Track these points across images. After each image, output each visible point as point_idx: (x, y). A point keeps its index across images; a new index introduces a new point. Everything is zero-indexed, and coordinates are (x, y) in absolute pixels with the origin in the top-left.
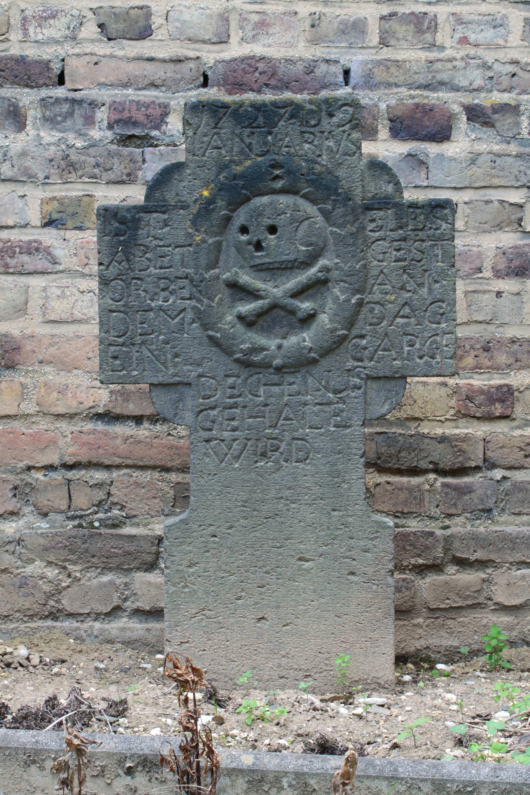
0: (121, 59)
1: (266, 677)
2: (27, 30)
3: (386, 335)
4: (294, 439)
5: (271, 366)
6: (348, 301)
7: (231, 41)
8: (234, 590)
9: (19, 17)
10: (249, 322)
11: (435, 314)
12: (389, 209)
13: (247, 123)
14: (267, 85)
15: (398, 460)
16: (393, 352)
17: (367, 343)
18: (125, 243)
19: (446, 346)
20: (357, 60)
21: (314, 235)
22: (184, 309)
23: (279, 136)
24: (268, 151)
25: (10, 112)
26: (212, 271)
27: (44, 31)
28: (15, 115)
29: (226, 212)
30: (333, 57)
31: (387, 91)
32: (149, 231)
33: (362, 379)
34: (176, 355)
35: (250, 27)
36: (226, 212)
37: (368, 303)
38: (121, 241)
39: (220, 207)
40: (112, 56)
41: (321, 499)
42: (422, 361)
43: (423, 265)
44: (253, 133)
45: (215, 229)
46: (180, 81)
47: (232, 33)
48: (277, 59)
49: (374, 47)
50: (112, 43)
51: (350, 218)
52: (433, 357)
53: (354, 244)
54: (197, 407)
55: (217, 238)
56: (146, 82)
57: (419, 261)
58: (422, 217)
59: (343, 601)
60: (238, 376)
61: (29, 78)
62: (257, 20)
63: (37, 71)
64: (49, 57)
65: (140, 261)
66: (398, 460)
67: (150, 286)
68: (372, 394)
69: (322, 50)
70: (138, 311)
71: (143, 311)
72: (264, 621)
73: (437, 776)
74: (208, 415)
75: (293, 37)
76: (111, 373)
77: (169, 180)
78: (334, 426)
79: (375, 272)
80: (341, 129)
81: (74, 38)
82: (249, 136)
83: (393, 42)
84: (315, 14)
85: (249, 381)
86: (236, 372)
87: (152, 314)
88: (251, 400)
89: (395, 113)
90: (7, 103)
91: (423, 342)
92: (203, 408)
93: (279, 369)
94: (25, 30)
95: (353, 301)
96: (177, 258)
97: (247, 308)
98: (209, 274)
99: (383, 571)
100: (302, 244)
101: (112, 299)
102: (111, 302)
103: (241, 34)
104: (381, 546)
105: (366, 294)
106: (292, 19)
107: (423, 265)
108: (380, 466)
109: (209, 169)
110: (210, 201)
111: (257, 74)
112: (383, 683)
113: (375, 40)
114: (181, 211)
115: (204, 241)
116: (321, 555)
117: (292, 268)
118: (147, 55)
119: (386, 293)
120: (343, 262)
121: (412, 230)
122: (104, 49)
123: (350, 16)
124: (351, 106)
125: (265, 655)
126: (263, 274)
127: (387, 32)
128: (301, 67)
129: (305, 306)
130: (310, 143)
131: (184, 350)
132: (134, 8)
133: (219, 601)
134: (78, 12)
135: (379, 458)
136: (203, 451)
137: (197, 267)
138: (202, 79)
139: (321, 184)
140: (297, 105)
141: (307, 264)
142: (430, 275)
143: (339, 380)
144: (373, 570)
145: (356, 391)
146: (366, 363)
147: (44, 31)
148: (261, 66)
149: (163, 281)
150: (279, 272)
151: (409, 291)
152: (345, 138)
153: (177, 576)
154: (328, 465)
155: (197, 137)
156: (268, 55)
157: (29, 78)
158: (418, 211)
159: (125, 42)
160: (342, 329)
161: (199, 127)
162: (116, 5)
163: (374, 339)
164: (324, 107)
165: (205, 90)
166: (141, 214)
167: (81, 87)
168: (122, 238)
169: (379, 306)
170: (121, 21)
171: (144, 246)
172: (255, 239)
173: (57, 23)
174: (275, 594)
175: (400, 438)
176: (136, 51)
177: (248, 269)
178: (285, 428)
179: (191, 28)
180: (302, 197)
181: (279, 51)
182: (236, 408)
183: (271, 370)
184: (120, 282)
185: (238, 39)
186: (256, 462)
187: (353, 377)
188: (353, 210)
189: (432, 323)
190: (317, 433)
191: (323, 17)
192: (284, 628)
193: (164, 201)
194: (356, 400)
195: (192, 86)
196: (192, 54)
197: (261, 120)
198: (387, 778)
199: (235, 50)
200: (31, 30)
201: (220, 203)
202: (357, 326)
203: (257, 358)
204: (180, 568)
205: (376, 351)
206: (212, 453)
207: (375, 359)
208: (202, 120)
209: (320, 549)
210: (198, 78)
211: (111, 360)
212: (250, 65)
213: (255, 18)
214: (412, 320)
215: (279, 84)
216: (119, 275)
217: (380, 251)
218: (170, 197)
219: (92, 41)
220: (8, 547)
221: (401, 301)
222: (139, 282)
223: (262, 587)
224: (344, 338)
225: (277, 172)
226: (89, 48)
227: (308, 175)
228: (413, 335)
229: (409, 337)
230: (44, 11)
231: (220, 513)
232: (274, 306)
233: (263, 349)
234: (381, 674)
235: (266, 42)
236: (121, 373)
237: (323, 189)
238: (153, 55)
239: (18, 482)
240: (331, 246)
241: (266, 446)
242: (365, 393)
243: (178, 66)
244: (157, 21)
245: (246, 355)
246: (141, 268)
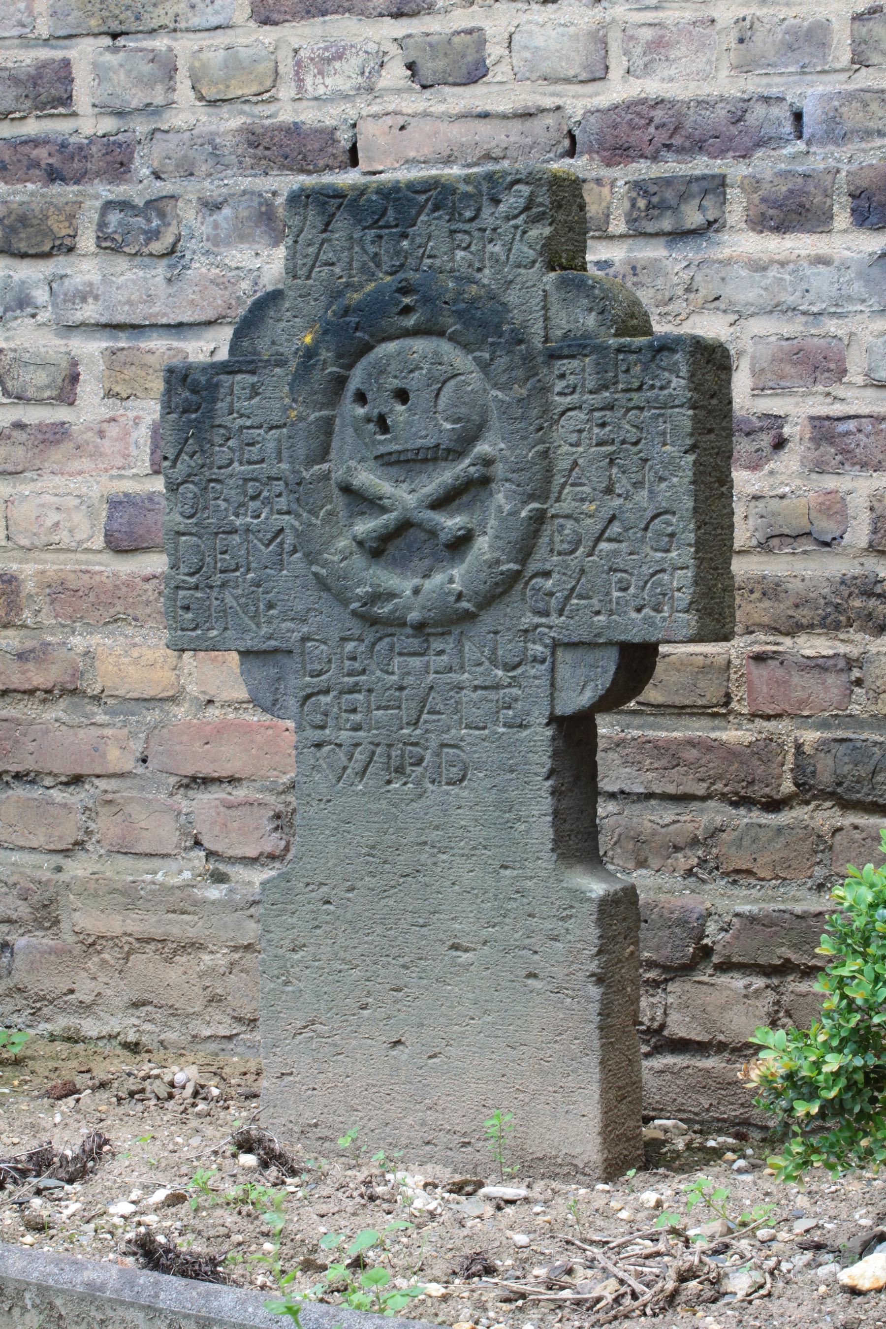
0: (439, 117)
1: (404, 1141)
2: (302, 80)
3: (582, 571)
4: (443, 745)
5: (404, 624)
6: (514, 513)
7: (610, 75)
8: (357, 993)
9: (290, 62)
10: (378, 549)
11: (660, 534)
12: (586, 356)
13: (370, 221)
14: (668, 147)
15: (874, 789)
16: (595, 601)
17: (554, 585)
18: (196, 424)
19: (679, 590)
20: (813, 94)
21: (464, 403)
22: (282, 530)
23: (418, 240)
24: (402, 265)
25: (262, 213)
26: (317, 467)
27: (328, 81)
28: (270, 219)
29: (334, 369)
30: (774, 91)
31: (864, 145)
32: (232, 403)
33: (546, 646)
34: (270, 606)
35: (639, 50)
36: (334, 369)
37: (553, 516)
38: (191, 421)
39: (325, 362)
40: (426, 114)
41: (485, 847)
42: (640, 616)
43: (640, 451)
44: (380, 237)
45: (319, 397)
46: (531, 148)
47: (613, 63)
48: (683, 102)
49: (843, 70)
50: (427, 93)
51: (520, 373)
52: (657, 609)
53: (523, 418)
54: (302, 689)
55: (324, 413)
56: (478, 153)
57: (636, 444)
58: (638, 368)
59: (519, 1022)
60: (360, 640)
61: (304, 159)
62: (649, 38)
63: (317, 146)
64: (334, 123)
65: (222, 454)
66: (874, 789)
67: (233, 492)
68: (563, 671)
69: (757, 80)
70: (217, 534)
71: (224, 532)
72: (401, 1047)
73: (204, 1313)
74: (317, 704)
75: (709, 62)
76: (179, 633)
77: (262, 319)
78: (504, 726)
79: (565, 464)
80: (512, 223)
81: (370, 89)
82: (373, 242)
83: (875, 59)
84: (744, 19)
85: (377, 648)
86: (356, 632)
87: (237, 538)
88: (379, 679)
89: (858, 182)
90: (256, 200)
91: (641, 583)
92: (309, 691)
93: (420, 627)
94: (300, 80)
95: (523, 514)
96: (271, 445)
97: (365, 526)
98: (311, 472)
99: (580, 974)
100: (446, 420)
101: (181, 514)
102: (181, 519)
103: (625, 64)
104: (578, 932)
105: (550, 502)
106: (708, 31)
107: (640, 451)
108: (841, 798)
109: (316, 300)
110: (310, 353)
111: (652, 129)
112: (581, 1166)
113: (845, 57)
114: (277, 370)
115: (301, 418)
116: (485, 943)
117: (435, 459)
118: (479, 109)
119: (583, 500)
120: (509, 448)
121: (623, 391)
122: (415, 102)
123: (803, 19)
124: (527, 183)
125: (402, 1104)
126: (393, 471)
127: (866, 42)
128: (724, 112)
129: (451, 523)
130: (465, 249)
131: (282, 597)
132: (459, 33)
133: (334, 1010)
134: (376, 47)
135: (839, 784)
136: (312, 762)
137: (293, 460)
138: (567, 143)
139: (473, 318)
140: (444, 186)
141: (455, 453)
142: (651, 468)
143: (510, 647)
144: (566, 971)
145: (537, 666)
146: (554, 620)
147: (328, 81)
148: (659, 115)
149: (251, 484)
150: (418, 466)
151: (619, 495)
152: (518, 238)
153: (275, 964)
154: (494, 791)
155: (298, 247)
156: (668, 95)
157: (304, 159)
158: (633, 357)
159: (447, 89)
160: (509, 562)
161: (301, 231)
162: (432, 30)
163: (564, 578)
164: (484, 188)
165: (571, 161)
166: (222, 377)
167: (381, 168)
168: (194, 416)
169: (572, 522)
170: (441, 55)
171: (225, 427)
172: (376, 411)
173: (345, 67)
174: (417, 1003)
175: (876, 749)
176: (463, 103)
177: (372, 463)
178: (429, 726)
179: (547, 58)
180: (450, 339)
181: (686, 88)
182: (359, 691)
183: (409, 631)
184: (191, 486)
185: (622, 72)
186: (389, 782)
187: (534, 642)
188: (524, 359)
189: (656, 550)
190: (476, 737)
191: (757, 25)
192: (431, 1061)
193: (255, 353)
194: (537, 682)
195: (551, 155)
196: (548, 102)
197: (391, 215)
198: (142, 1308)
199: (618, 90)
200: (309, 81)
201: (325, 354)
202: (537, 557)
203: (383, 610)
204: (280, 952)
205: (568, 598)
206: (325, 766)
207: (566, 613)
208: (305, 218)
209: (484, 932)
210: (559, 142)
211: (180, 612)
212: (640, 115)
213: (647, 34)
214: (624, 545)
215: (687, 144)
216: (189, 475)
217: (571, 428)
218: (264, 347)
219: (399, 91)
220: (252, 910)
221: (606, 514)
222: (218, 487)
223: (398, 990)
224: (516, 576)
225: (407, 300)
226: (392, 103)
227: (455, 302)
228: (625, 571)
229: (619, 575)
230: (326, 49)
231: (335, 865)
232: (405, 526)
233: (391, 595)
234: (578, 1150)
235: (666, 73)
236: (194, 634)
237: (481, 324)
238: (488, 108)
239: (281, 807)
240: (495, 422)
241: (402, 756)
242: (553, 670)
243: (529, 123)
244: (494, 51)
245: (365, 604)
246: (220, 463)
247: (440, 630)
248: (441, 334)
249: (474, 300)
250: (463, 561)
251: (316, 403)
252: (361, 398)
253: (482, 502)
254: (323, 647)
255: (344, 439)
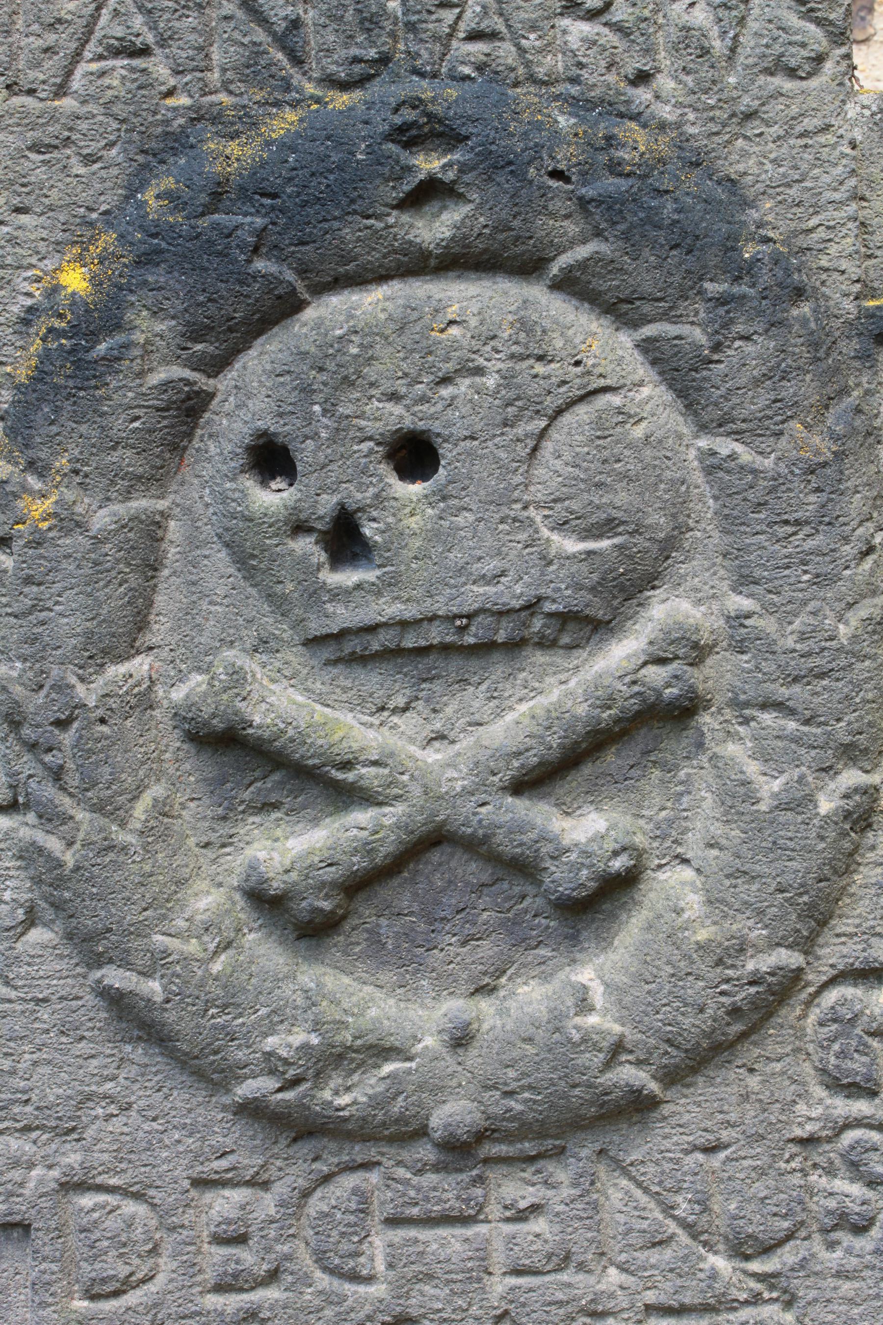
6: (798, 803)
29: (178, 372)
36: (178, 372)
39: (147, 349)
53: (825, 519)
55: (140, 504)
86: (249, 1162)
88: (329, 1298)
95: (826, 805)
97: (294, 846)
98: (99, 683)
100: (561, 526)
109: (89, 159)
110: (97, 320)
115: (68, 521)
117: (514, 646)
126: (372, 681)
139: (652, 221)
141: (582, 627)
143: (760, 1189)
145: (845, 1237)
150: (454, 665)
177: (294, 656)
187: (830, 1172)
194: (847, 1287)
201: (147, 327)
224: (783, 988)
225: (429, 164)
232: (430, 841)
247: (528, 1147)
248: (529, 267)
249: (643, 172)
250: (605, 942)
251: (114, 475)
252: (270, 458)
253: (670, 769)
254: (130, 1207)
255: (198, 585)
